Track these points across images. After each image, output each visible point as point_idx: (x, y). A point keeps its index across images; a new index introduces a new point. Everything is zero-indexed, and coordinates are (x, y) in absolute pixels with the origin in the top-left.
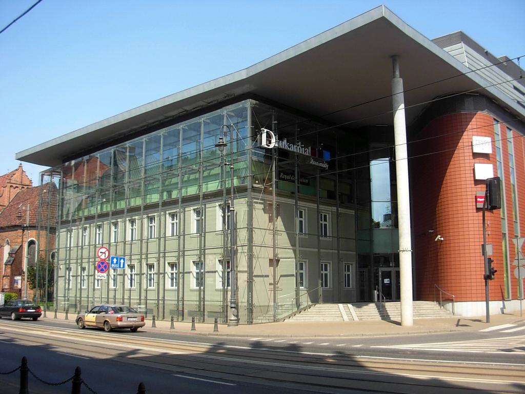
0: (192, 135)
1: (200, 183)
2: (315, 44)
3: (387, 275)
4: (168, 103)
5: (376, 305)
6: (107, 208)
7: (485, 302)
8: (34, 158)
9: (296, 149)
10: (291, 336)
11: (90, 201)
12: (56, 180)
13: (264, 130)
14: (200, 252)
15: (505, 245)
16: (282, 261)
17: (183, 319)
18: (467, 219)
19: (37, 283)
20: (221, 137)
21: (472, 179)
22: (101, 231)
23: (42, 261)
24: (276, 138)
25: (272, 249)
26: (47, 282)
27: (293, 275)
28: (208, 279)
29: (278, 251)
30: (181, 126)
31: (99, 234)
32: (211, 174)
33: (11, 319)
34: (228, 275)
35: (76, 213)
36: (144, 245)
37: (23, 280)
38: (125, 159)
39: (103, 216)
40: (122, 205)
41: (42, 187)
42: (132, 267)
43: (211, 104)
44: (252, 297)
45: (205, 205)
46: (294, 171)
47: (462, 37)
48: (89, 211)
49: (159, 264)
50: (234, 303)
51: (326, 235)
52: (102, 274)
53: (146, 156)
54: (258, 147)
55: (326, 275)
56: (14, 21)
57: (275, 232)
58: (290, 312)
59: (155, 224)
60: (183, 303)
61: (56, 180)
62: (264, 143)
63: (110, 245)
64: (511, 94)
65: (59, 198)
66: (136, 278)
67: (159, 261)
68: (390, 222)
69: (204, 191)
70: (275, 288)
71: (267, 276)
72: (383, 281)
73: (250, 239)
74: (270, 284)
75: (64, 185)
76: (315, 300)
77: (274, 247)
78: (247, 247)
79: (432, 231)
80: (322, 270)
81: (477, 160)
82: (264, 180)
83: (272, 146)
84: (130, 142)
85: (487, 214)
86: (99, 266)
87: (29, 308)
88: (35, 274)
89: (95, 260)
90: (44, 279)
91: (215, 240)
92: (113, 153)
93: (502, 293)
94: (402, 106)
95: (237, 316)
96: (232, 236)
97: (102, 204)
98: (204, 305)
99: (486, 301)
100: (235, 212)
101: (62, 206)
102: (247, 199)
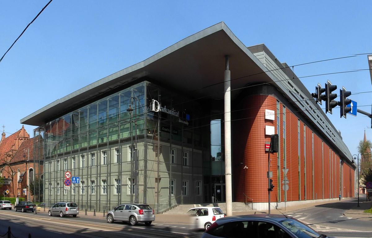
1: (118, 133)
3: (219, 188)
5: (213, 204)
6: (70, 149)
7: (268, 203)
9: (170, 112)
11: (61, 145)
13: (154, 101)
14: (119, 174)
15: (279, 172)
16: (162, 180)
20: (130, 105)
23: (37, 180)
24: (160, 106)
25: (157, 172)
26: (39, 192)
27: (168, 188)
29: (160, 174)
30: (108, 98)
32: (124, 128)
33: (22, 212)
35: (53, 152)
36: (89, 170)
37: (27, 190)
38: (78, 119)
39: (67, 153)
40: (77, 147)
41: (35, 138)
42: (83, 182)
45: (121, 146)
47: (264, 48)
48: (60, 151)
49: (97, 180)
52: (68, 187)
53: (89, 117)
54: (150, 111)
55: (185, 188)
57: (159, 163)
58: (166, 209)
59: (95, 158)
60: (110, 202)
61: (42, 133)
62: (154, 109)
64: (286, 86)
65: (44, 144)
67: (97, 179)
68: (220, 157)
69: (121, 138)
70: (158, 195)
71: (154, 188)
72: (217, 191)
73: (146, 166)
75: (46, 135)
76: (179, 202)
77: (158, 171)
79: (242, 163)
80: (183, 185)
81: (267, 123)
82: (153, 131)
83: (158, 111)
84: (80, 109)
85: (271, 155)
86: (66, 182)
87: (30, 206)
88: (34, 187)
89: (64, 178)
90: (38, 190)
91: (126, 167)
92: (71, 116)
93: (276, 198)
94: (229, 89)
96: (136, 165)
97: (67, 146)
99: (269, 202)
100: (138, 150)
101: (46, 149)
102: (144, 143)
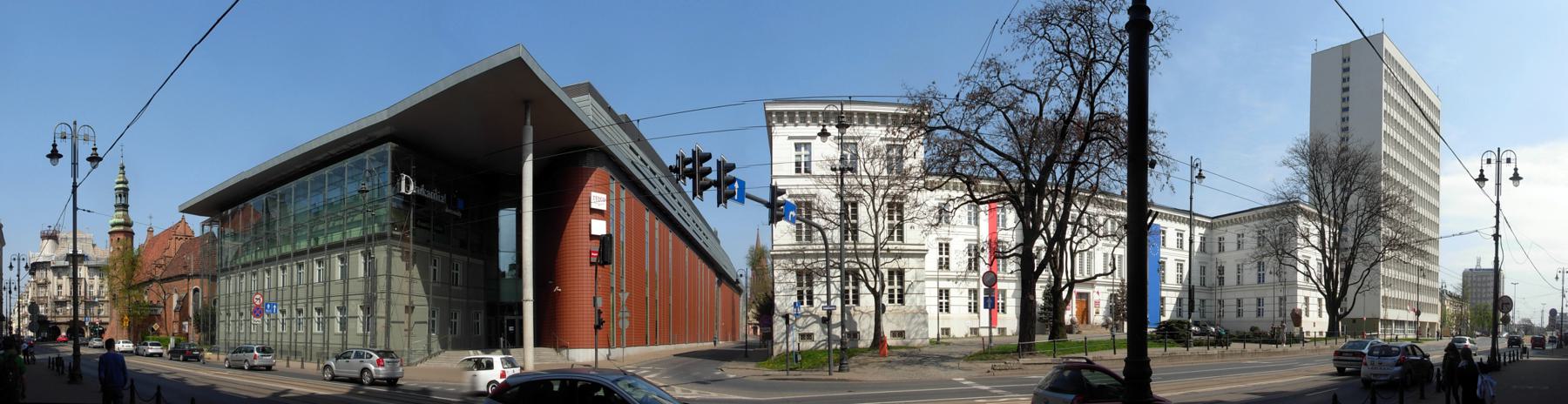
3: (511, 323)
6: (261, 256)
8: (194, 209)
9: (432, 196)
12: (215, 229)
29: (414, 298)
36: (294, 291)
37: (190, 324)
39: (258, 263)
40: (274, 252)
42: (283, 312)
47: (589, 89)
48: (245, 259)
51: (456, 285)
53: (295, 203)
57: (411, 280)
59: (303, 270)
61: (215, 229)
62: (403, 191)
68: (514, 272)
70: (409, 333)
71: (403, 322)
72: (508, 328)
73: (389, 286)
74: (405, 330)
75: (222, 233)
76: (444, 347)
77: (410, 295)
78: (385, 294)
81: (593, 216)
83: (410, 193)
85: (599, 268)
90: (207, 324)
91: (357, 287)
94: (530, 157)
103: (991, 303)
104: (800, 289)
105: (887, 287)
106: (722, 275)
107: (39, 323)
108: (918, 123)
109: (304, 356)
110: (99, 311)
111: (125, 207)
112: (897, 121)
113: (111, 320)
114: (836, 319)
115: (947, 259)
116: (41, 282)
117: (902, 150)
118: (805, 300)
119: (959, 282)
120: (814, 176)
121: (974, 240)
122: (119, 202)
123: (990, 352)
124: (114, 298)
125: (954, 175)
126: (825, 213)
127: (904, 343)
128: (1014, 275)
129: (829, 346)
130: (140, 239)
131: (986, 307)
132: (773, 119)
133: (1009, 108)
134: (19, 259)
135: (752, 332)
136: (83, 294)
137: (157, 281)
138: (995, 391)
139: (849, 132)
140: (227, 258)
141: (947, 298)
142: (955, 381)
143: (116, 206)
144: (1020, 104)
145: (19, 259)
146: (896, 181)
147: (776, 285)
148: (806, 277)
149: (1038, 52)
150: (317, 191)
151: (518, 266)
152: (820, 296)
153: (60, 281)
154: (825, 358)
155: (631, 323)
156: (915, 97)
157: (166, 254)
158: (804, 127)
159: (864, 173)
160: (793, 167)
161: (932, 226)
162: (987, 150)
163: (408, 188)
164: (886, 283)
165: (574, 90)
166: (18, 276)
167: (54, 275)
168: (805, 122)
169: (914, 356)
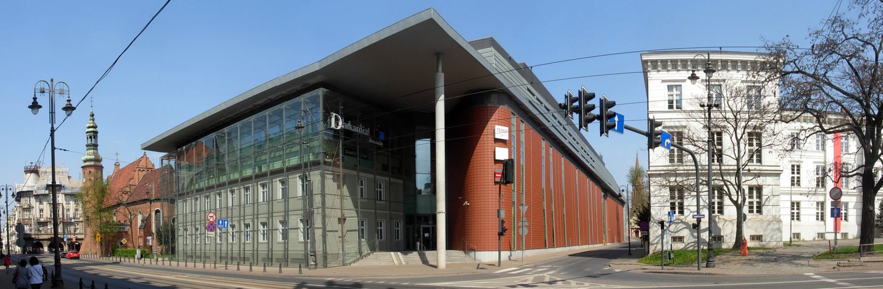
0: (276, 119)
2: (375, 39)
3: (426, 230)
4: (256, 94)
5: (418, 253)
6: (213, 182)
8: (155, 147)
9: (358, 130)
10: (356, 277)
12: (172, 162)
13: (333, 114)
17: (272, 265)
18: (487, 170)
19: (163, 241)
21: (493, 159)
22: (209, 200)
23: (166, 224)
26: (170, 240)
27: (356, 230)
28: (291, 234)
29: (345, 212)
30: (267, 112)
31: (207, 202)
34: (308, 230)
36: (242, 209)
37: (153, 239)
39: (210, 188)
40: (224, 179)
41: (163, 169)
42: (233, 227)
43: (291, 92)
44: (326, 247)
46: (356, 148)
47: (492, 43)
48: (199, 185)
50: (313, 252)
51: (381, 200)
52: (212, 233)
53: (240, 139)
54: (328, 129)
55: (381, 230)
56: (135, 39)
57: (342, 197)
58: (355, 259)
59: (250, 193)
61: (172, 162)
62: (333, 126)
63: (216, 210)
66: (236, 235)
67: (253, 221)
68: (429, 189)
70: (342, 240)
71: (337, 231)
72: (424, 235)
73: (324, 202)
74: (339, 237)
75: (178, 166)
76: (373, 249)
77: (342, 209)
78: (321, 209)
80: (378, 226)
81: (497, 144)
82: (333, 156)
83: (339, 128)
85: (503, 186)
88: (162, 234)
90: (168, 238)
91: (296, 204)
94: (442, 97)
95: (315, 262)
98: (288, 254)
103: (836, 213)
104: (672, 201)
105: (748, 200)
106: (607, 191)
107: (25, 240)
108: (774, 68)
109: (251, 261)
110: (75, 230)
111: (95, 146)
112: (756, 67)
113: (85, 236)
114: (704, 224)
115: (798, 178)
116: (26, 207)
117: (761, 90)
118: (677, 210)
119: (810, 196)
120: (685, 111)
121: (823, 163)
122: (89, 142)
123: (834, 252)
124: (87, 219)
125: (806, 110)
126: (694, 141)
127: (761, 245)
128: (855, 191)
129: (698, 246)
130: (108, 171)
131: (832, 215)
132: (646, 67)
133: (851, 57)
134: (7, 189)
135: (634, 235)
136: (61, 216)
137: (123, 205)
138: (840, 284)
139: (715, 76)
140: (183, 185)
141: (798, 209)
142: (805, 275)
143: (87, 146)
144: (861, 54)
145: (7, 189)
146: (756, 115)
147: (652, 198)
148: (678, 191)
149: (871, 11)
150: (259, 128)
151: (432, 185)
152: (689, 207)
153: (41, 206)
154: (694, 256)
155: (529, 233)
156: (772, 47)
157: (131, 183)
158: (676, 72)
159: (728, 109)
160: (667, 104)
161: (787, 151)
162: (834, 90)
163: (337, 124)
164: (747, 197)
165: (480, 44)
166: (6, 202)
167: (36, 201)
168: (666, 68)
169: (769, 256)
